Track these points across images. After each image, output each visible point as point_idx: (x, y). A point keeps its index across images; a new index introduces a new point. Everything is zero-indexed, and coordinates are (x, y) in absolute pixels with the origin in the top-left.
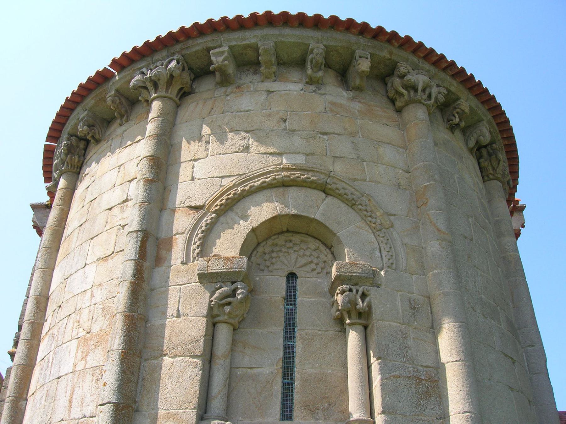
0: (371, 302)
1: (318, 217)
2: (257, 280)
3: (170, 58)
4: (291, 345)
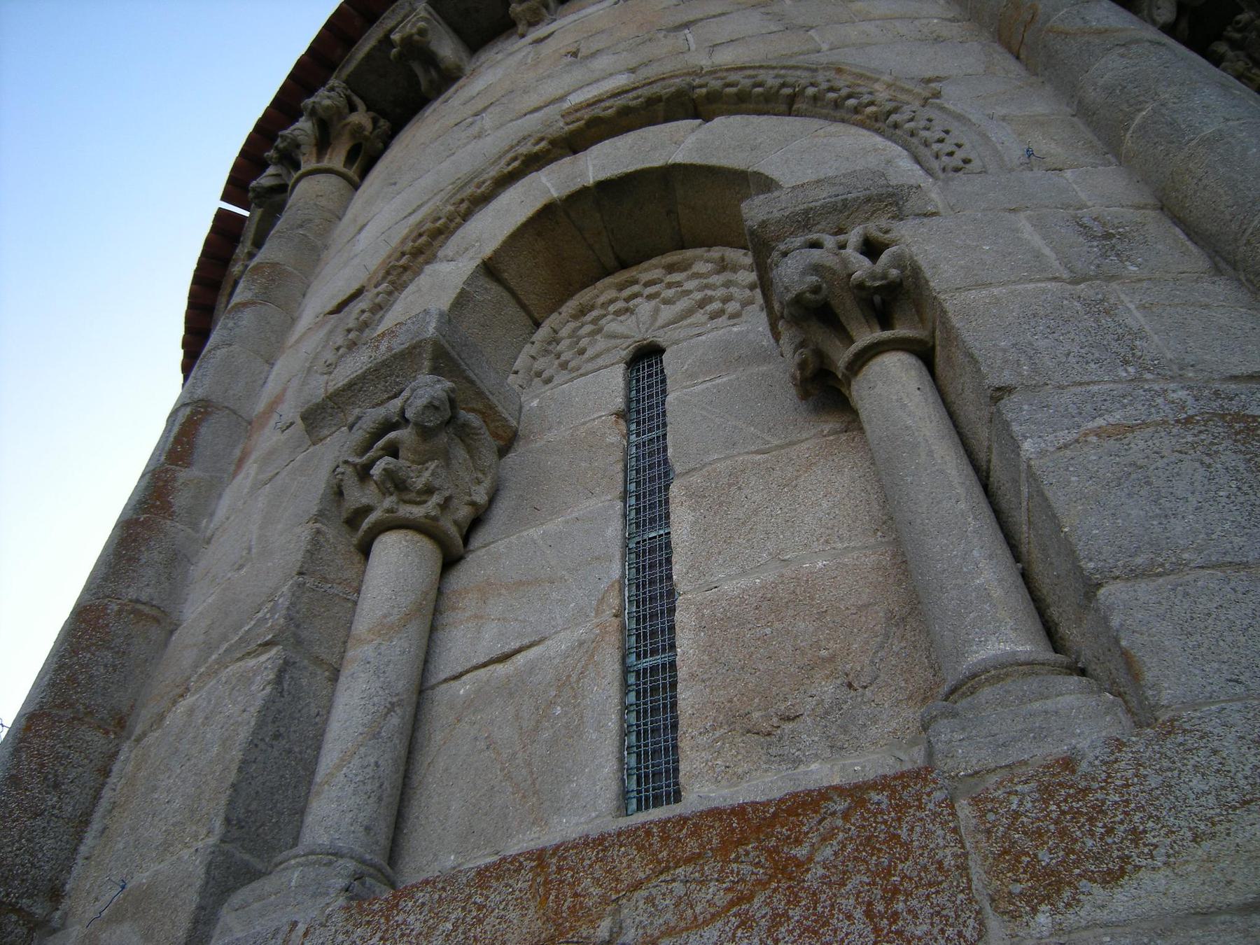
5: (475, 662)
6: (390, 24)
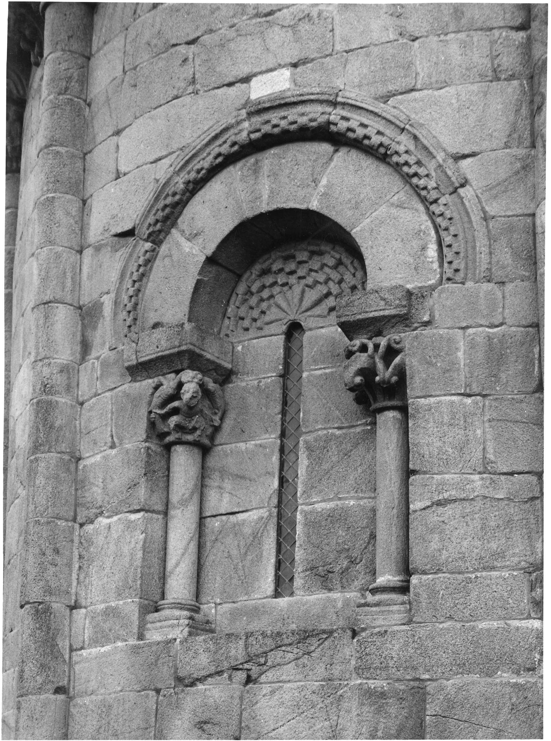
0: (405, 364)
2: (238, 351)
5: (221, 512)
6: (137, 252)
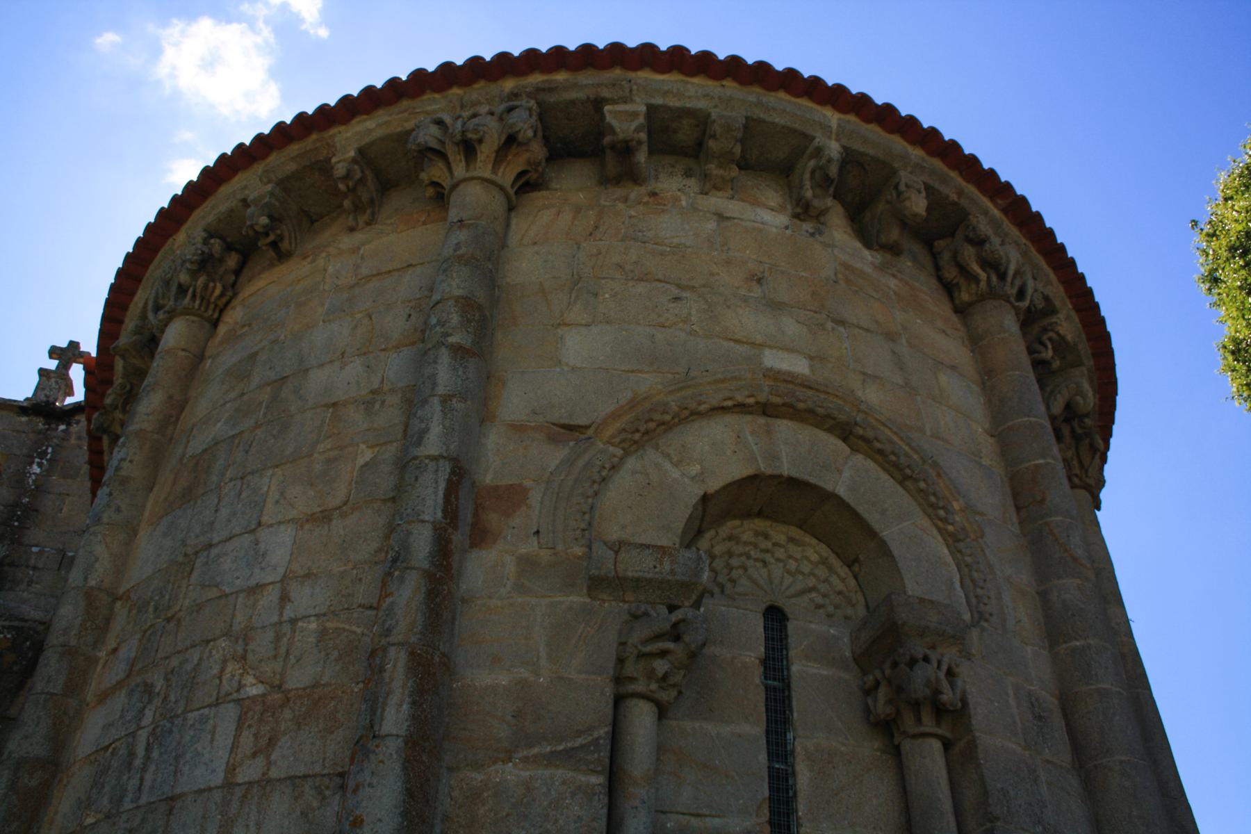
1: (841, 491)
3: (511, 103)
4: (782, 769)
